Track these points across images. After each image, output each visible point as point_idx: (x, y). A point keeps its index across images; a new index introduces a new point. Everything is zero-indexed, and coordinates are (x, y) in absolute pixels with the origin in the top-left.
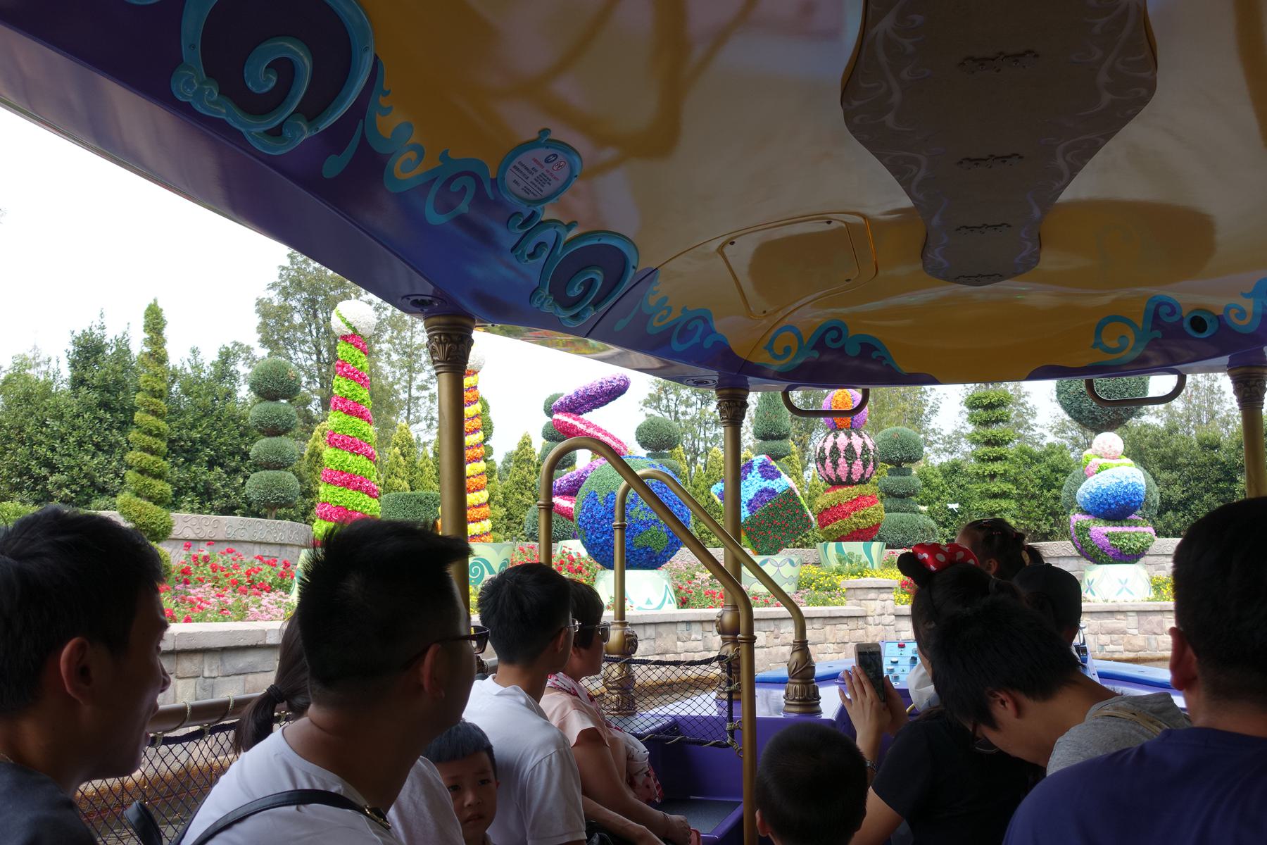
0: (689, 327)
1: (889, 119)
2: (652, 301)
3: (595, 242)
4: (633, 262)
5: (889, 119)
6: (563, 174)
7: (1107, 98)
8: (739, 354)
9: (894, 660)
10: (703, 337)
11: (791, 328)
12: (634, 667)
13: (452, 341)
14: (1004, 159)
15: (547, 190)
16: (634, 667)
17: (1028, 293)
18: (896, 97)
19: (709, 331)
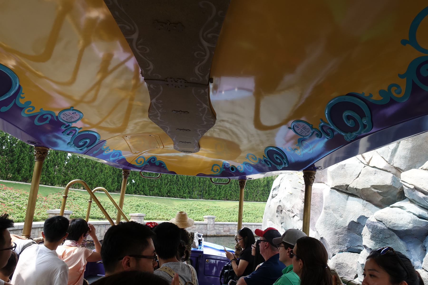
0: (44, 117)
1: (159, 118)
2: (104, 147)
3: (87, 133)
4: (98, 138)
5: (159, 118)
6: (78, 117)
7: (205, 123)
8: (128, 161)
9: (295, 187)
11: (143, 157)
13: (41, 154)
15: (73, 120)
18: (159, 115)
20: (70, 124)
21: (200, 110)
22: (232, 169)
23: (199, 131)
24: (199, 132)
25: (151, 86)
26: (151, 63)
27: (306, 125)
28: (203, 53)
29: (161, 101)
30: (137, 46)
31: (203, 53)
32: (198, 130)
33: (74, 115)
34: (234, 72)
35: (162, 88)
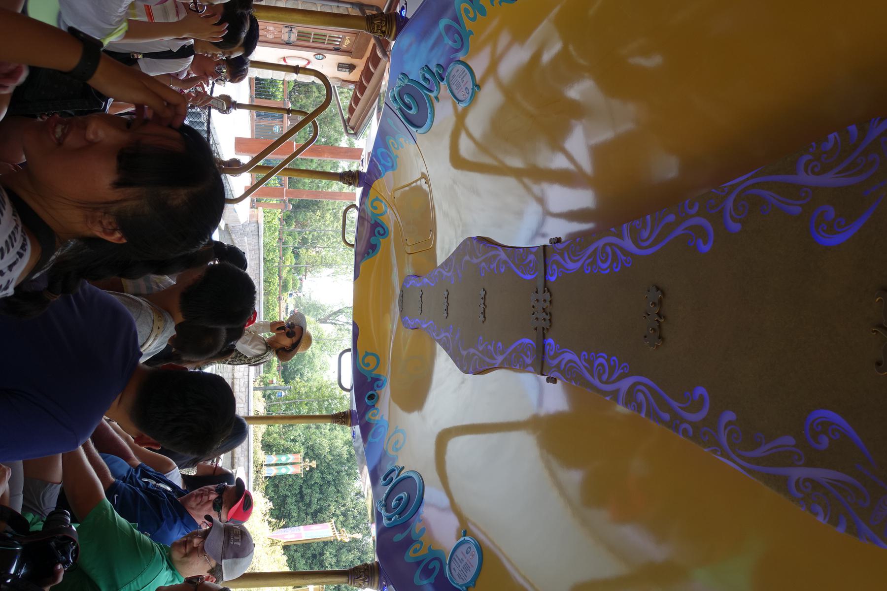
1: (467, 258)
3: (429, 111)
4: (420, 131)
6: (460, 97)
7: (464, 353)
10: (383, 165)
12: (214, 95)
14: (447, 310)
15: (454, 87)
16: (214, 95)
17: (393, 321)
18: (475, 261)
19: (387, 169)
20: (445, 82)
21: (490, 347)
22: (371, 397)
23: (446, 337)
24: (443, 335)
25: (532, 257)
26: (578, 265)
27: (473, 570)
28: (605, 377)
29: (503, 270)
30: (611, 245)
31: (605, 377)
32: (448, 334)
33: (464, 89)
34: (572, 395)
35: (529, 277)
